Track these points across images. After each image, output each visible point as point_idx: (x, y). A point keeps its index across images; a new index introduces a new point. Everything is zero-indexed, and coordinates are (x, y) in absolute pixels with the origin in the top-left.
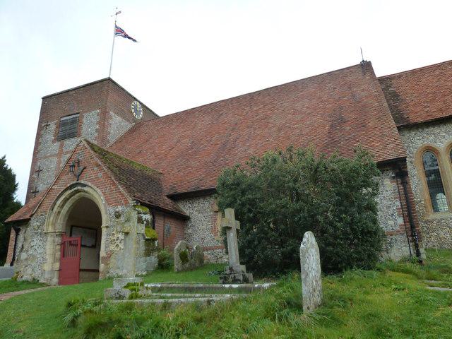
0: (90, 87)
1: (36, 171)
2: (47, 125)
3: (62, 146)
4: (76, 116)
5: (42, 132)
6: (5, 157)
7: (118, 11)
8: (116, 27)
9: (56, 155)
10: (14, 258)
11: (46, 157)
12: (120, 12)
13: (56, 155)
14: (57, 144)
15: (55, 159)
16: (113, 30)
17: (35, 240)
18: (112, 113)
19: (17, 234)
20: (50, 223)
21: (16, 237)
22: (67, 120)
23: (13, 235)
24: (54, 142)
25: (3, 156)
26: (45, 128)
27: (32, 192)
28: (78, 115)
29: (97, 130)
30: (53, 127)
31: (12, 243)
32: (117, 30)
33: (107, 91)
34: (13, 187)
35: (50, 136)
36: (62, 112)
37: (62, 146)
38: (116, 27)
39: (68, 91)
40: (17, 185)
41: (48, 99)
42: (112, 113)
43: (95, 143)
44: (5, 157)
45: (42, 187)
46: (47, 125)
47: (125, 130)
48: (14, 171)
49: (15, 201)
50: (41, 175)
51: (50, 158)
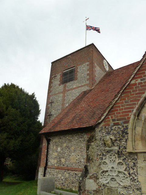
0: (80, 51)
1: (50, 103)
2: (55, 76)
4: (74, 68)
5: (53, 81)
6: (34, 93)
7: (87, 18)
8: (87, 26)
9: (62, 92)
10: (51, 168)
11: (55, 94)
12: (88, 19)
13: (62, 92)
14: (62, 86)
15: (61, 95)
16: (85, 27)
17: (107, 161)
18: (96, 65)
19: (48, 144)
20: (138, 137)
21: (48, 146)
22: (67, 71)
23: (45, 144)
24: (60, 85)
25: (85, 26)
26: (54, 78)
27: (48, 115)
28: (74, 68)
29: (88, 74)
30: (59, 76)
31: (44, 151)
32: (87, 28)
33: (92, 51)
34: (38, 112)
35: (57, 82)
36: (64, 70)
37: (65, 86)
38: (87, 26)
39: (67, 56)
40: (40, 111)
41: (55, 63)
42: (96, 65)
44: (34, 93)
45: (53, 112)
46: (55, 76)
47: (103, 76)
48: (39, 103)
49: (38, 120)
50: (53, 104)
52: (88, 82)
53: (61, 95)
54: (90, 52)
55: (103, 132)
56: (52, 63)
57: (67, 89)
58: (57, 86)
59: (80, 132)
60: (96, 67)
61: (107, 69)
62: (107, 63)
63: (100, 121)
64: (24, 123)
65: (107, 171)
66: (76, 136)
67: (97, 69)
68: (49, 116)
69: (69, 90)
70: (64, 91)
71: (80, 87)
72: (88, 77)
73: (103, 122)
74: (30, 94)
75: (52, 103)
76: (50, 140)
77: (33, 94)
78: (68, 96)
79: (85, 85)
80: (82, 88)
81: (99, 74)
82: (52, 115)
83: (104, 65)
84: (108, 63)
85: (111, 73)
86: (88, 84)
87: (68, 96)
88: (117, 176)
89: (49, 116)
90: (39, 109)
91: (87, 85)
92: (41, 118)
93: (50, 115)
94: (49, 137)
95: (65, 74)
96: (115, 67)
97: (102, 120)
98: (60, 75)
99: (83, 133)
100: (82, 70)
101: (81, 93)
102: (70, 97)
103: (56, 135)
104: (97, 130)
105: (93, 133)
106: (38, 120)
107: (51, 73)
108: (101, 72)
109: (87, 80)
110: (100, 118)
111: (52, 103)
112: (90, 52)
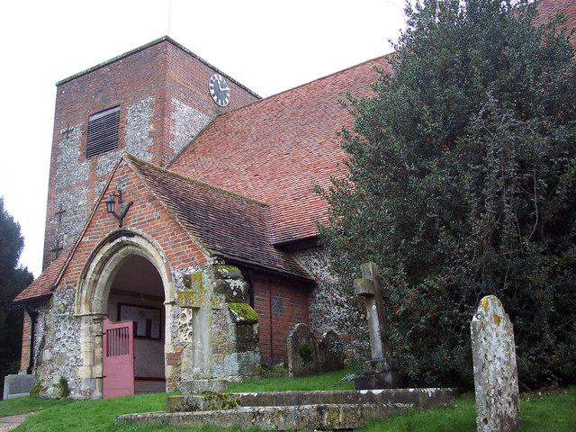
1: (57, 214)
14: (86, 164)
19: (34, 322)
20: (83, 301)
23: (27, 324)
24: (80, 161)
29: (151, 135)
30: (78, 134)
35: (74, 151)
39: (99, 67)
46: (68, 132)
49: (18, 267)
50: (64, 219)
56: (60, 85)
57: (100, 173)
58: (75, 162)
65: (60, 339)
68: (53, 251)
75: (61, 213)
76: (37, 314)
84: (226, 77)
88: (67, 341)
89: (53, 251)
93: (58, 250)
94: (35, 307)
95: (91, 128)
98: (82, 128)
106: (18, 267)
109: (149, 151)
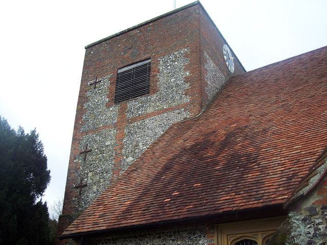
1: (81, 152)
2: (96, 83)
3: (123, 111)
5: (88, 94)
13: (115, 125)
14: (114, 109)
22: (130, 70)
24: (108, 106)
26: (92, 87)
27: (75, 189)
29: (187, 80)
30: (106, 84)
34: (42, 179)
35: (102, 96)
36: (121, 69)
39: (129, 30)
40: (49, 172)
41: (94, 48)
43: (216, 234)
46: (96, 83)
48: (47, 152)
49: (57, 220)
51: (103, 131)
52: (187, 100)
53: (113, 132)
54: (186, 30)
55: (317, 221)
59: (186, 231)
60: (207, 63)
61: (232, 69)
62: (230, 54)
63: (305, 190)
64: (173, 137)
66: (173, 240)
67: (210, 65)
69: (134, 120)
70: (123, 122)
71: (166, 111)
72: (187, 86)
73: (316, 194)
74: (27, 132)
75: (86, 152)
77: (33, 132)
78: (132, 134)
79: (178, 107)
80: (172, 114)
81: (213, 79)
82: (86, 185)
83: (225, 57)
85: (238, 82)
86: (187, 104)
87: (132, 134)
89: (76, 188)
90: (46, 167)
91: (185, 106)
92: (53, 198)
96: (250, 65)
97: (311, 186)
98: (110, 79)
99: (194, 234)
100: (171, 72)
101: (167, 127)
102: (136, 137)
103: (113, 239)
104: (296, 219)
105: (281, 227)
107: (83, 73)
108: (219, 74)
109: (186, 94)
110: (305, 180)
111: (86, 152)
112: (186, 30)
